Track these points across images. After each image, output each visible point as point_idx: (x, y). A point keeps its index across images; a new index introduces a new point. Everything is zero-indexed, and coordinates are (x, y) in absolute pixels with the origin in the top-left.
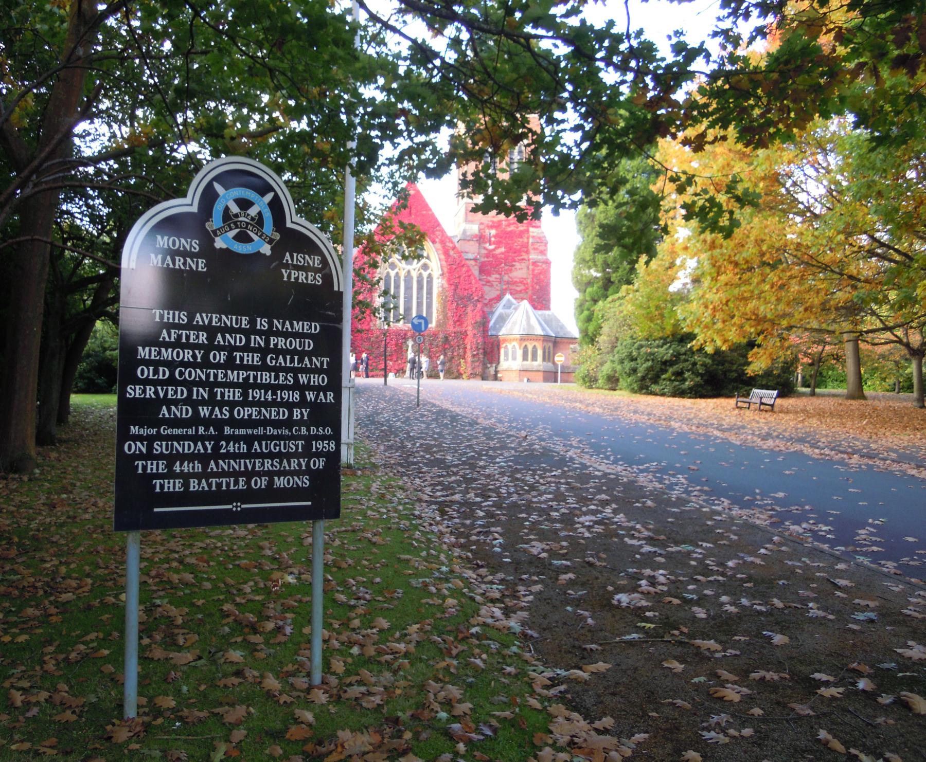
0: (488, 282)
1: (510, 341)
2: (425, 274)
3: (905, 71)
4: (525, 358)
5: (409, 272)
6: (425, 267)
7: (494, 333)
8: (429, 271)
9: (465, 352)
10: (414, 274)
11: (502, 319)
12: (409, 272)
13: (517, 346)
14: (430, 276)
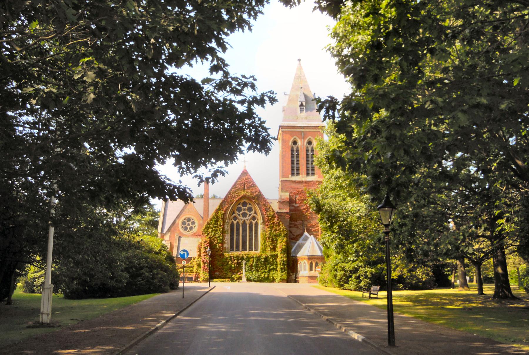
0: (296, 225)
1: (303, 259)
2: (235, 222)
3: (326, 12)
4: (311, 269)
5: (244, 221)
6: (254, 218)
7: (294, 255)
8: (256, 221)
9: (277, 267)
10: (248, 223)
11: (300, 247)
12: (244, 221)
13: (306, 262)
14: (238, 223)
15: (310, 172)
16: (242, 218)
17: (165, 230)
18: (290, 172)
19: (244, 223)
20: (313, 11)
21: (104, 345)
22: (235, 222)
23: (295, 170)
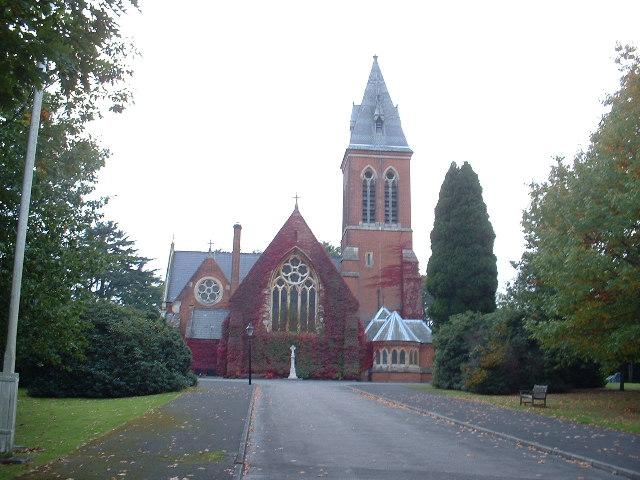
2: (280, 289)
15: (391, 218)
16: (291, 282)
17: (173, 298)
18: (360, 216)
19: (294, 292)
20: (376, 82)
21: (247, 403)
22: (280, 289)
23: (368, 214)
